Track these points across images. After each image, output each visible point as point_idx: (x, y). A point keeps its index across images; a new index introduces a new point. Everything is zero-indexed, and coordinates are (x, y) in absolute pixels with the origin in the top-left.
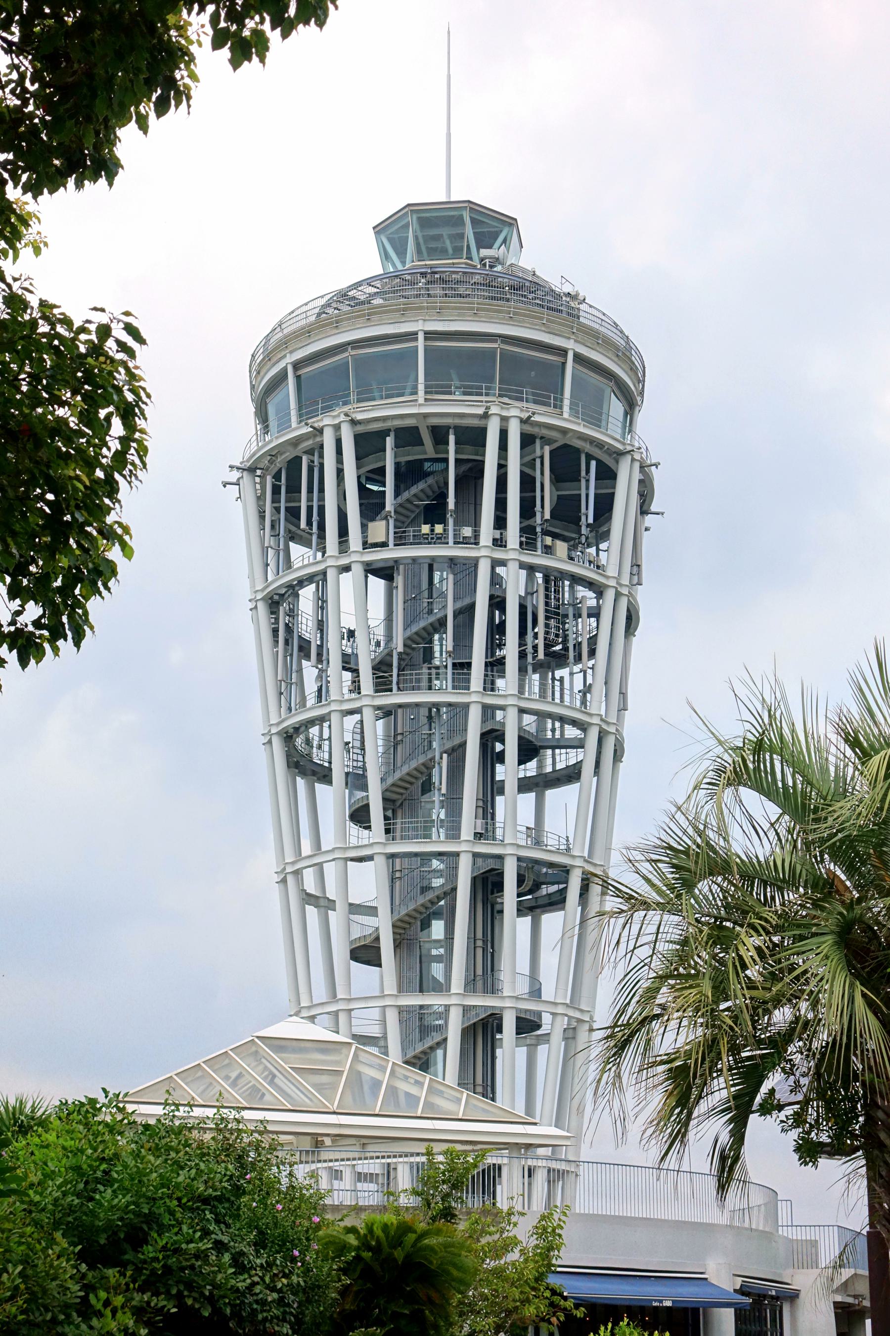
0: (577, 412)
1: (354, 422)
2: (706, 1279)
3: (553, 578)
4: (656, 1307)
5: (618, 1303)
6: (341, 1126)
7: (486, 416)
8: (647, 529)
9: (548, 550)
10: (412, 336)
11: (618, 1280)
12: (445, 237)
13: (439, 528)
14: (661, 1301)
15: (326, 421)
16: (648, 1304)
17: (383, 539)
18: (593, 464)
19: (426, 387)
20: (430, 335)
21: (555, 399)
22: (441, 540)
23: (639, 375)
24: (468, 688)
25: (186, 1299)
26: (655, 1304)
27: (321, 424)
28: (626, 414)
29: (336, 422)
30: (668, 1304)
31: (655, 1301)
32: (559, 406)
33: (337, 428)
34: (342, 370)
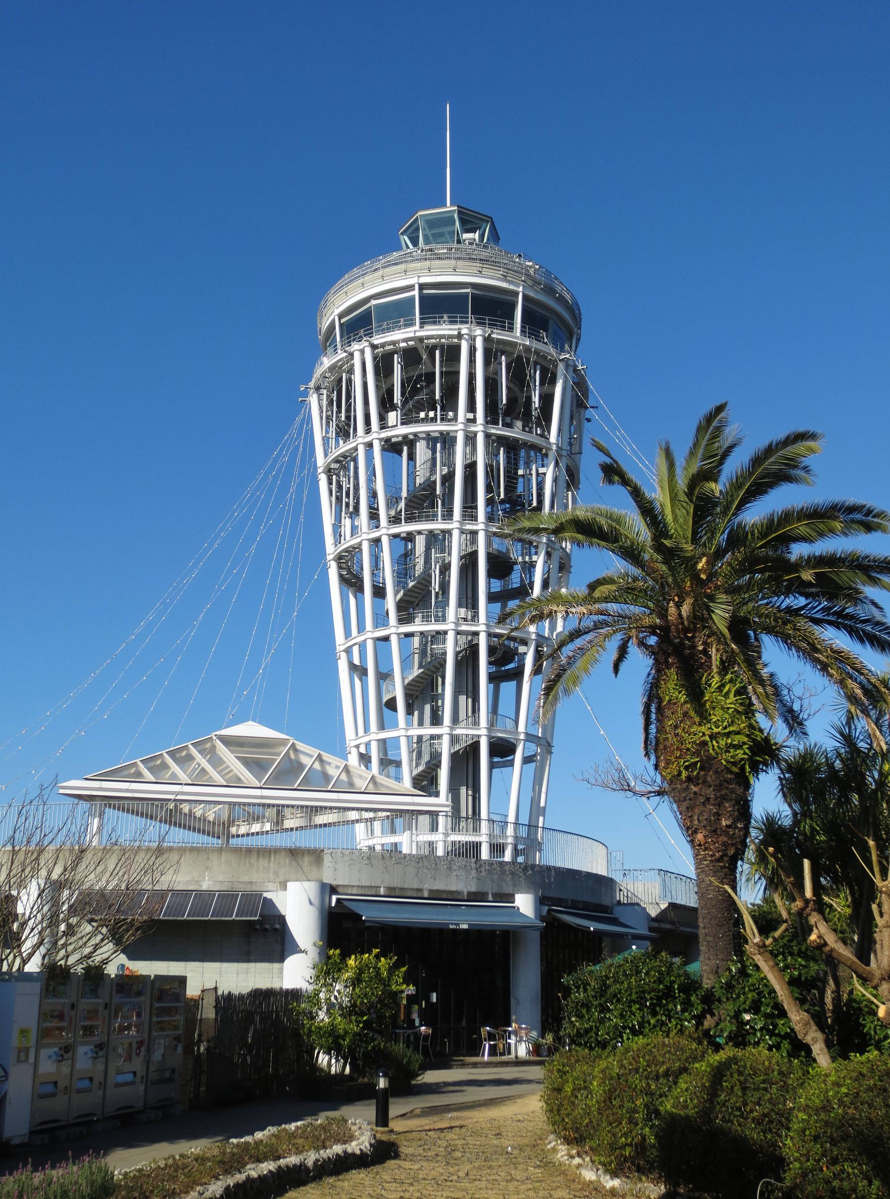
0: (525, 332)
1: (374, 347)
2: (514, 907)
3: (512, 447)
4: (454, 930)
5: (433, 926)
6: (262, 797)
7: (460, 336)
8: (589, 420)
9: (509, 425)
10: (410, 288)
11: (430, 909)
12: (446, 233)
13: (431, 414)
14: (458, 924)
15: (355, 347)
16: (445, 927)
17: (395, 424)
18: (538, 367)
19: (421, 319)
20: (422, 287)
21: (509, 323)
22: (434, 420)
23: (577, 319)
24: (452, 520)
25: (694, 995)
26: (451, 927)
27: (352, 350)
28: (668, 447)
29: (362, 347)
30: (465, 926)
31: (452, 924)
32: (511, 329)
33: (362, 352)
34: (368, 313)
